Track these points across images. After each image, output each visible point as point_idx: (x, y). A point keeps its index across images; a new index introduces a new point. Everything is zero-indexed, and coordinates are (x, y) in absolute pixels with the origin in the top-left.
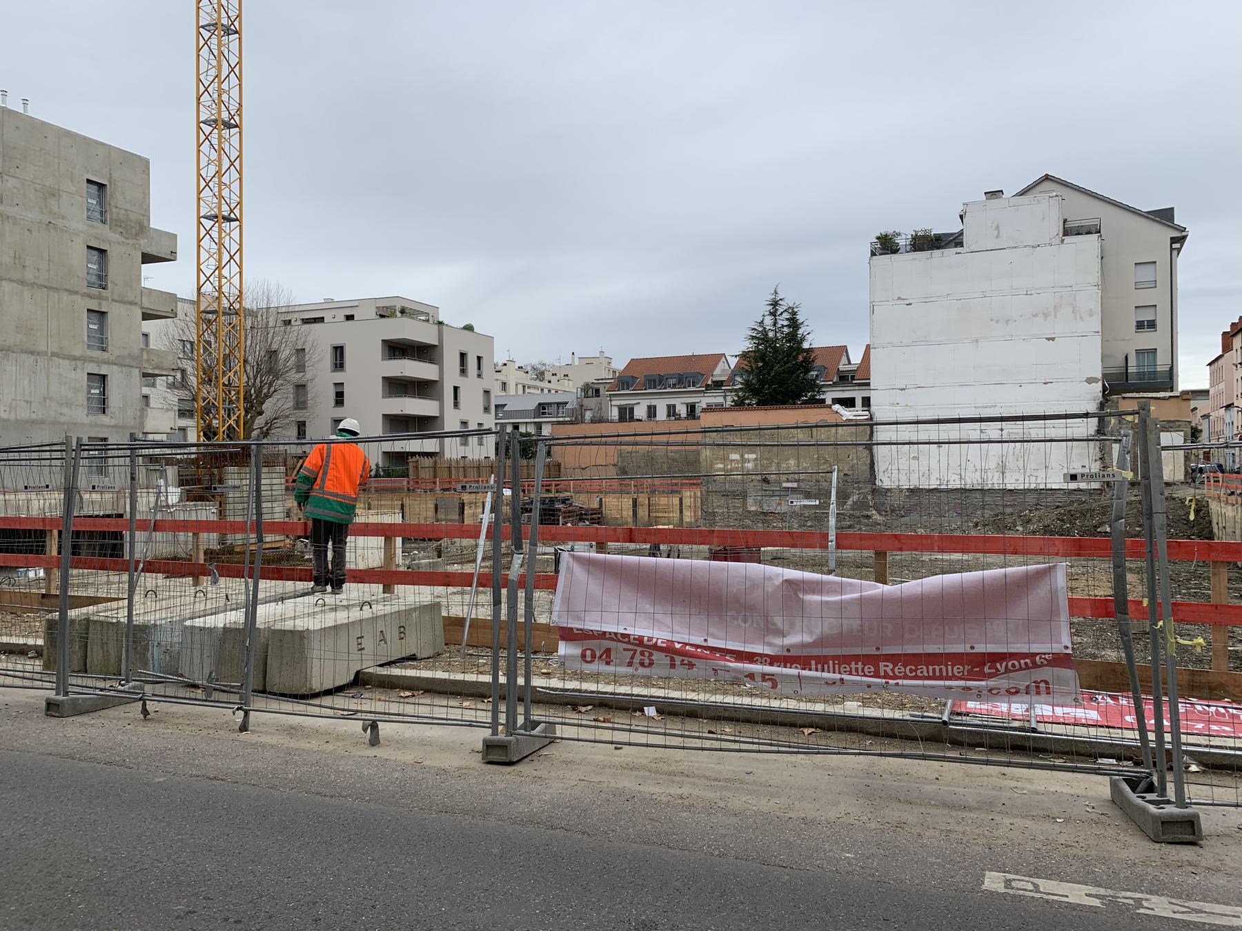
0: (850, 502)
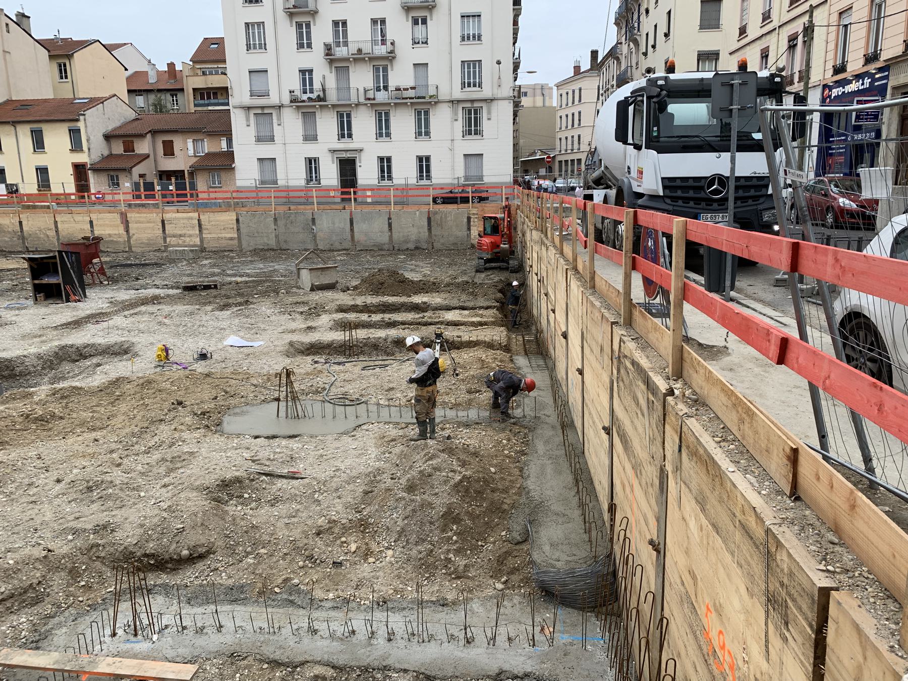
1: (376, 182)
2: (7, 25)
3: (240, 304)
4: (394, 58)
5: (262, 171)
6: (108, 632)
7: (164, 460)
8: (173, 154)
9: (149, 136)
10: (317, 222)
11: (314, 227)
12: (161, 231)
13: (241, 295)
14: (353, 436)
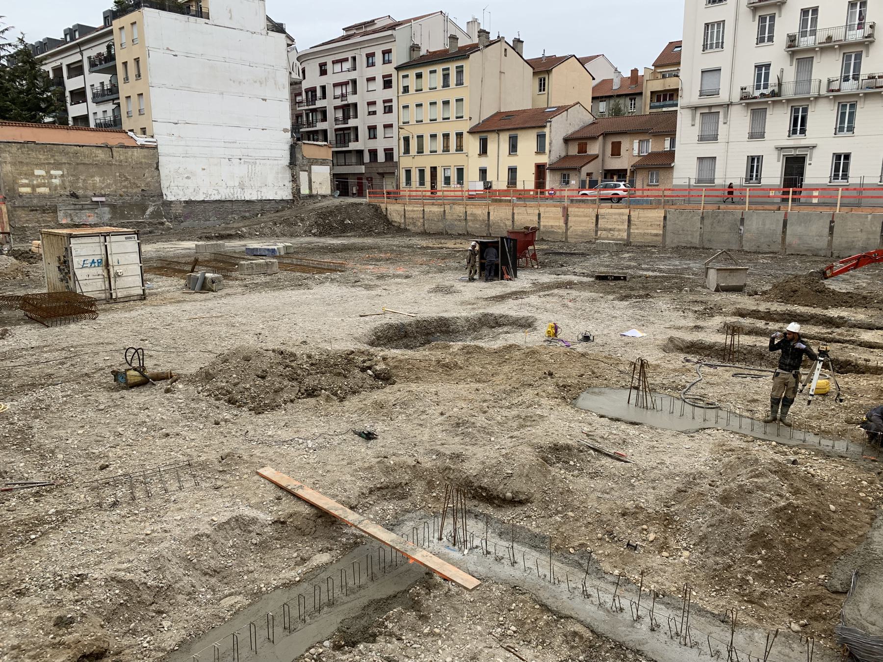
0: (148, 212)
1: (827, 181)
2: (506, 50)
3: (640, 297)
4: (872, 42)
5: (700, 170)
6: (436, 535)
7: (519, 416)
8: (620, 155)
9: (601, 138)
10: (746, 222)
11: (742, 228)
12: (594, 225)
13: (645, 288)
14: (692, 437)
